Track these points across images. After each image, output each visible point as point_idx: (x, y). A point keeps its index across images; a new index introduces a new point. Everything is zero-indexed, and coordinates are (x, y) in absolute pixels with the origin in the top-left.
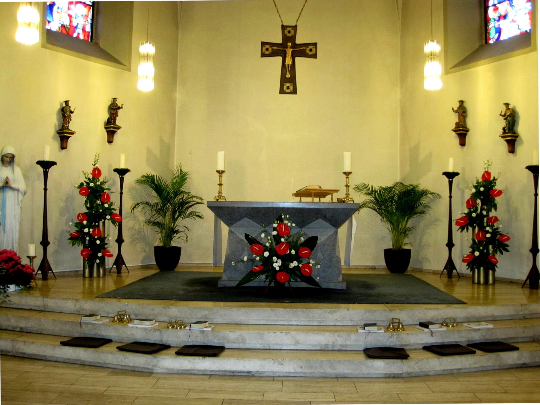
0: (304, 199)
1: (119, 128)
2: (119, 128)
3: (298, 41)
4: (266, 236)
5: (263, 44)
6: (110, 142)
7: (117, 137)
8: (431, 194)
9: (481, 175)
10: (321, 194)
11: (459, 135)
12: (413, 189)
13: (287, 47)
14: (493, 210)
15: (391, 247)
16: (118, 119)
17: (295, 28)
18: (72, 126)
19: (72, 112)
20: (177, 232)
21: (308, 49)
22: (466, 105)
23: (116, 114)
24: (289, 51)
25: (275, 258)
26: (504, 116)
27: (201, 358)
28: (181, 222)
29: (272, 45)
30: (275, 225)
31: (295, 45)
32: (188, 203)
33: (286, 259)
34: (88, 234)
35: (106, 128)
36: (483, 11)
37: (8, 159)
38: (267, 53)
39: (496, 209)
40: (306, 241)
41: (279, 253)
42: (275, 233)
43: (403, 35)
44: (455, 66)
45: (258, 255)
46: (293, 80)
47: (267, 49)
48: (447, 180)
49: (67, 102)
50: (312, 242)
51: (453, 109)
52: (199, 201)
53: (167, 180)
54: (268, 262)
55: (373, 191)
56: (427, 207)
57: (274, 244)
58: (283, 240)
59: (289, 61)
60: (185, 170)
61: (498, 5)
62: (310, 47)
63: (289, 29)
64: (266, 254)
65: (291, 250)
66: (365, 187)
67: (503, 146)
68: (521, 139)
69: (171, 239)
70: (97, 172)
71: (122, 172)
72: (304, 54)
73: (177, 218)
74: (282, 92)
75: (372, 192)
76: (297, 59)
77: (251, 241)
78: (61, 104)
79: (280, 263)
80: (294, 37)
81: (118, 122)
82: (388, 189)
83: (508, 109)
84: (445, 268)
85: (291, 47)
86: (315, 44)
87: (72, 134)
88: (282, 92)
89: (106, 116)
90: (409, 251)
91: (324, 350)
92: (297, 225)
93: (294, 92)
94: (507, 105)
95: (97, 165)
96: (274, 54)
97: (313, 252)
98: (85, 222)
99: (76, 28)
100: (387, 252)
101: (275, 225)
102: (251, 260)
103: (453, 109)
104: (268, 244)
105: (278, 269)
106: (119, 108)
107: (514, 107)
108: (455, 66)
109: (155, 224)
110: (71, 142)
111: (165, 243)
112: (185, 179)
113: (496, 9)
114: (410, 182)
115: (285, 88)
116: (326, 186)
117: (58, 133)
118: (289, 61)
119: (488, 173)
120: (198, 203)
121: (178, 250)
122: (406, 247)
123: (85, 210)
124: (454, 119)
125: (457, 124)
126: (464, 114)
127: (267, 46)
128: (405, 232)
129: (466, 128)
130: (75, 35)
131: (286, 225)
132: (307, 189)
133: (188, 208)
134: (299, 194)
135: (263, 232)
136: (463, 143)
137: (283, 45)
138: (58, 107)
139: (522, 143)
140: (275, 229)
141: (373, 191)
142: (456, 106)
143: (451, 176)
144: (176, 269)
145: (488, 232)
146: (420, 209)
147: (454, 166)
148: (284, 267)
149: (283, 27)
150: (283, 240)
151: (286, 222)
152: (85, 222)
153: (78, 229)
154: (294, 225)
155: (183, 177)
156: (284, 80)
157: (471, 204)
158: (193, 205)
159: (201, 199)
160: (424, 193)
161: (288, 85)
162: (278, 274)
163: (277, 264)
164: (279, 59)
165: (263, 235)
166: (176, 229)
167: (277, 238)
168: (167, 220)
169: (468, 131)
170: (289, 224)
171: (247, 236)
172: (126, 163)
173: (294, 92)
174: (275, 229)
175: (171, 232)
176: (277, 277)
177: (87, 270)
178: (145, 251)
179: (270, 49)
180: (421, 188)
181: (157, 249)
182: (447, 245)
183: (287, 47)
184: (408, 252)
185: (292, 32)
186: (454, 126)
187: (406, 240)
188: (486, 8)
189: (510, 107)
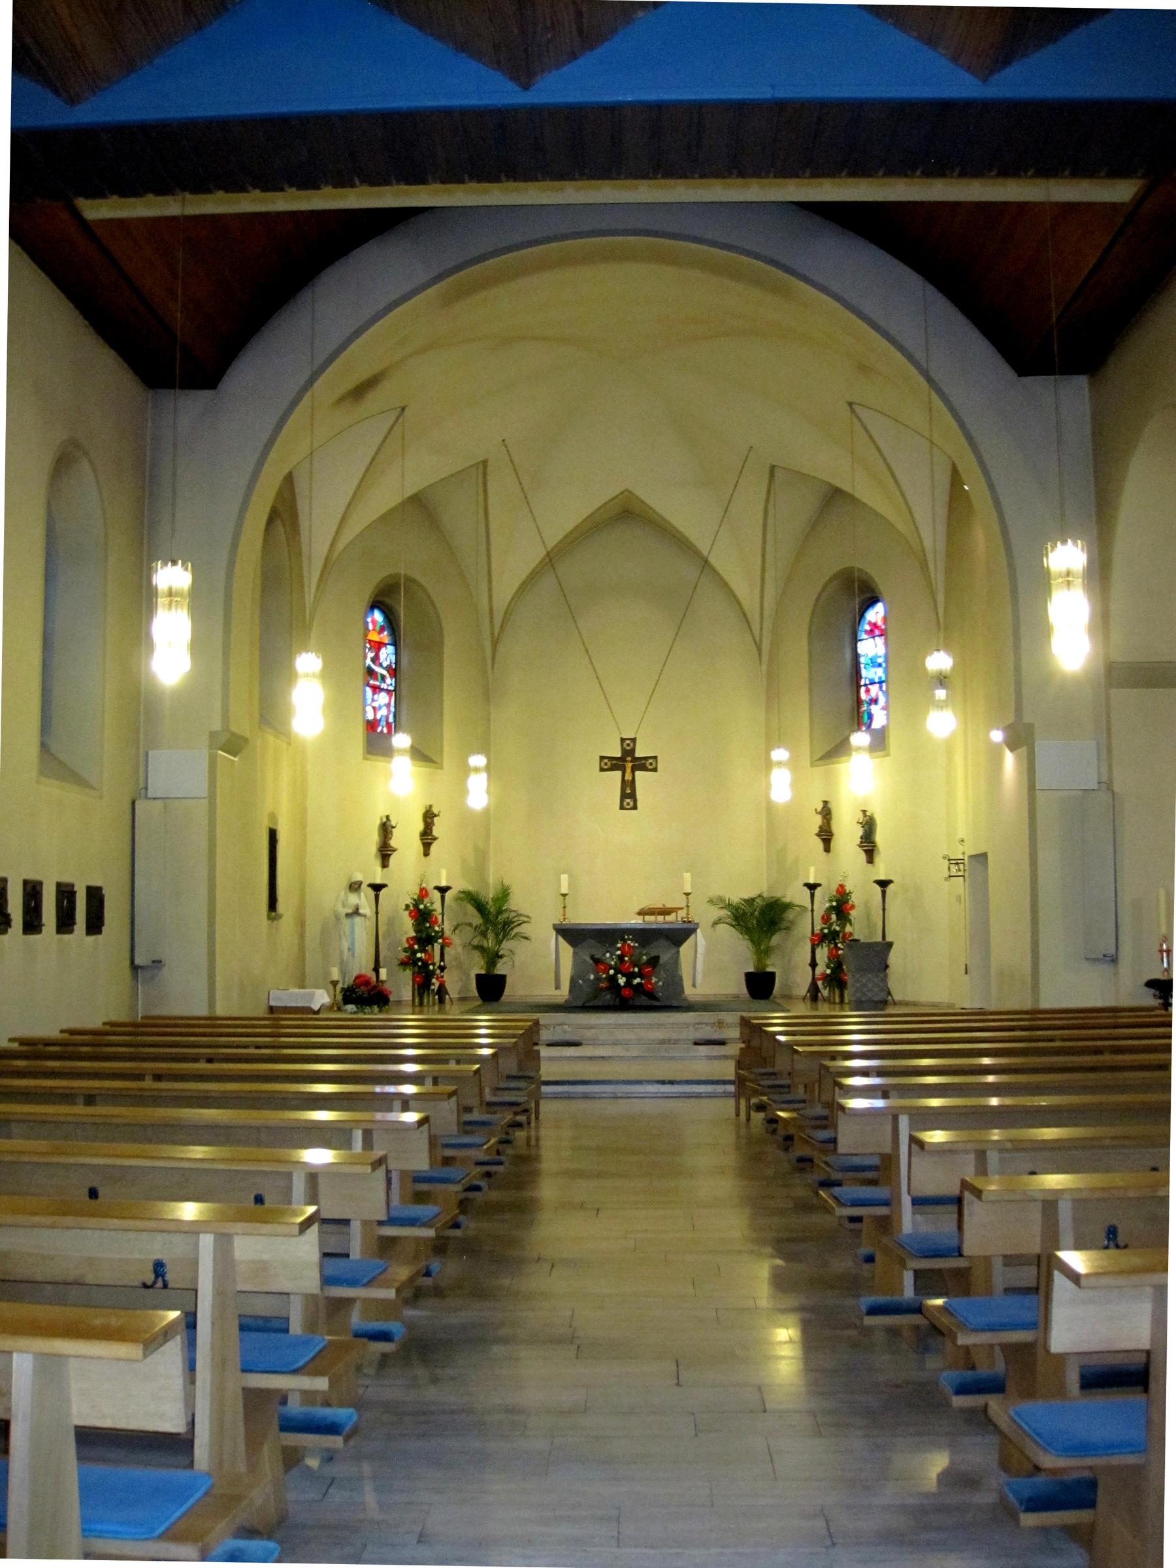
0: (647, 918)
1: (435, 839)
2: (435, 839)
3: (638, 754)
4: (611, 956)
5: (602, 758)
6: (426, 854)
7: (434, 848)
8: (797, 906)
9: (835, 890)
10: (665, 912)
11: (823, 840)
12: (777, 900)
13: (626, 761)
14: (848, 925)
15: (751, 970)
16: (434, 828)
17: (634, 740)
18: (393, 843)
19: (393, 827)
20: (501, 957)
21: (648, 763)
22: (832, 806)
23: (432, 824)
24: (629, 766)
25: (619, 976)
26: (861, 823)
27: (567, 1048)
28: (506, 945)
29: (611, 759)
30: (619, 945)
31: (635, 759)
32: (513, 922)
33: (630, 976)
34: (420, 959)
35: (421, 840)
36: (855, 689)
37: (357, 886)
38: (605, 767)
39: (851, 924)
40: (648, 960)
41: (623, 970)
42: (619, 952)
43: (769, 708)
44: (821, 759)
45: (604, 973)
46: (633, 796)
47: (606, 764)
48: (808, 891)
49: (388, 817)
50: (654, 961)
51: (816, 810)
52: (526, 919)
53: (489, 895)
54: (613, 979)
55: (729, 905)
56: (792, 922)
57: (618, 963)
58: (626, 959)
59: (628, 777)
60: (506, 882)
61: (869, 686)
62: (650, 761)
63: (628, 742)
64: (612, 972)
65: (634, 968)
66: (721, 899)
67: (863, 856)
68: (878, 850)
69: (495, 966)
70: (423, 893)
71: (443, 890)
72: (643, 768)
73: (502, 941)
74: (622, 808)
75: (729, 906)
76: (638, 773)
77: (597, 961)
78: (381, 819)
79: (624, 979)
80: (633, 750)
81: (435, 832)
82: (750, 902)
83: (865, 816)
84: (808, 991)
85: (631, 761)
86: (655, 758)
87: (395, 851)
88: (622, 808)
89: (421, 826)
90: (772, 975)
91: (663, 1042)
92: (639, 945)
93: (635, 808)
94: (864, 812)
95: (424, 885)
96: (612, 769)
97: (656, 969)
98: (416, 947)
99: (380, 720)
100: (749, 977)
101: (619, 945)
102: (598, 979)
103: (816, 810)
104: (613, 963)
105: (622, 984)
106: (435, 816)
107: (872, 814)
108: (821, 759)
109: (476, 947)
110: (393, 860)
111: (488, 969)
112: (508, 894)
113: (868, 691)
114: (778, 894)
115: (625, 804)
116: (669, 905)
117: (380, 851)
118: (628, 777)
119: (842, 886)
120: (524, 922)
121: (502, 979)
122: (770, 969)
123: (413, 934)
124: (818, 820)
125: (820, 827)
126: (828, 817)
127: (606, 761)
128: (767, 952)
129: (831, 832)
130: (379, 729)
131: (629, 945)
132: (650, 909)
133: (512, 929)
134: (642, 913)
135: (607, 952)
136: (827, 849)
137: (622, 759)
138: (378, 822)
139: (879, 853)
140: (618, 949)
141: (729, 905)
142: (820, 807)
143: (812, 887)
144: (503, 998)
145: (840, 949)
146: (783, 925)
147: (815, 879)
148: (628, 984)
149: (623, 740)
150: (626, 959)
151: (629, 942)
152: (416, 947)
153: (407, 954)
154: (636, 945)
155: (504, 894)
156: (624, 796)
157: (826, 919)
158: (519, 925)
159: (528, 917)
160: (788, 906)
161: (628, 800)
162: (623, 990)
163: (622, 981)
164: (618, 773)
165: (608, 955)
166: (500, 953)
167: (621, 958)
168: (490, 943)
169: (832, 836)
170: (632, 944)
171: (592, 957)
172: (447, 880)
173: (635, 808)
174: (618, 949)
175: (493, 958)
176: (622, 993)
177: (417, 1000)
178: (461, 980)
179: (609, 764)
180: (787, 900)
181: (478, 977)
182: (810, 965)
183: (626, 761)
184: (772, 975)
185: (632, 745)
186: (817, 830)
187: (768, 962)
188: (859, 687)
189: (868, 814)
